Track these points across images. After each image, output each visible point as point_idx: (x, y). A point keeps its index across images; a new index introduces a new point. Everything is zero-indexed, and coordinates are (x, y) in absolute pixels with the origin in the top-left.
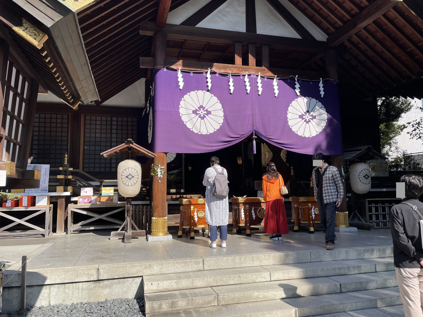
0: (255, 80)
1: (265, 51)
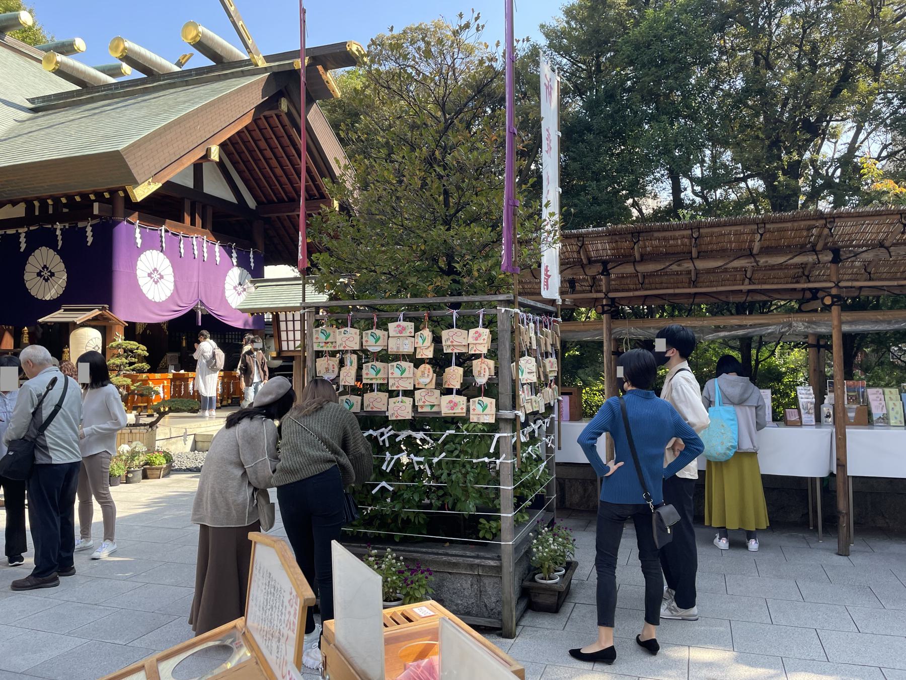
0: (203, 246)
1: (209, 212)
